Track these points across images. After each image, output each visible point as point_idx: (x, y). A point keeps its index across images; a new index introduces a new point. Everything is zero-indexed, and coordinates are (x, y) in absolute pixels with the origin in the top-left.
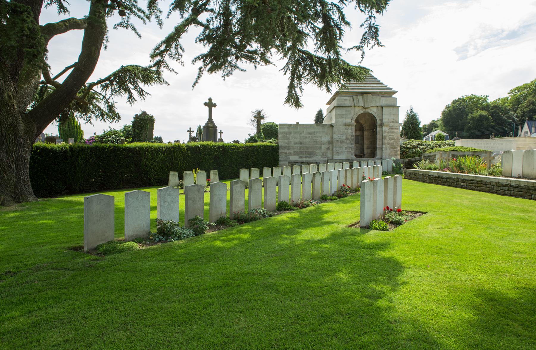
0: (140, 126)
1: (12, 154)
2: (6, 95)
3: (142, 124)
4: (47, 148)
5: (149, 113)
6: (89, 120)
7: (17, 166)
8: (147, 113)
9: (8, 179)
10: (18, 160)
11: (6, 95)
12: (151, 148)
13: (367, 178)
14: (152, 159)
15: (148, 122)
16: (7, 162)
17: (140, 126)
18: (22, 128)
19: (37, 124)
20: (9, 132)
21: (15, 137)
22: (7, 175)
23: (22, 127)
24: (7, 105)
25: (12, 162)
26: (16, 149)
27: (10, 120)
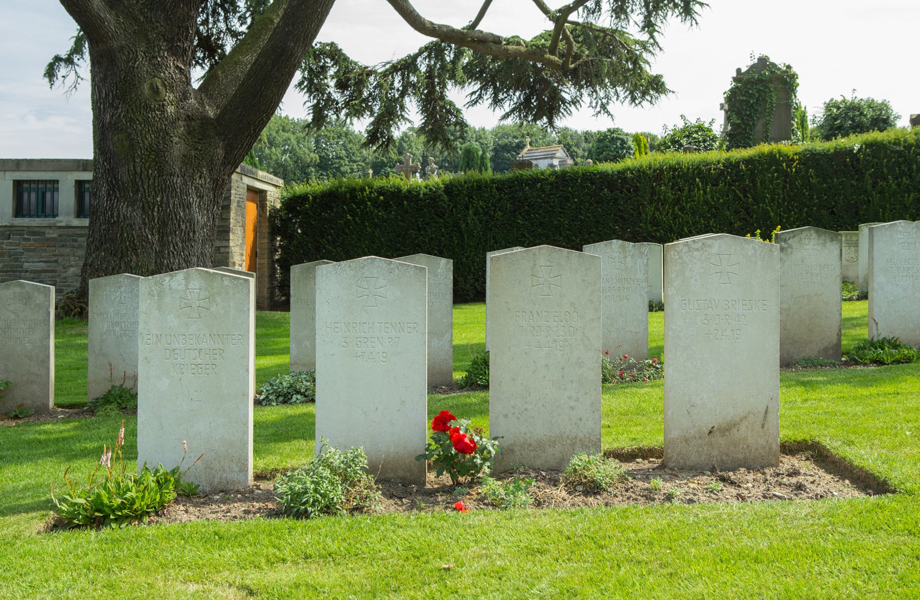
0: (747, 102)
1: (153, 211)
2: (146, 87)
3: (751, 96)
4: (399, 190)
5: (779, 59)
6: (603, 107)
7: (161, 240)
8: (772, 60)
9: (137, 265)
10: (164, 224)
11: (146, 87)
12: (672, 168)
13: (271, 461)
14: (677, 202)
15: (772, 86)
16: (140, 228)
17: (747, 102)
18: (177, 153)
19: (224, 140)
20: (147, 165)
21: (161, 174)
22: (137, 255)
23: (178, 147)
24: (148, 108)
25: (151, 229)
26: (161, 201)
27: (150, 138)
